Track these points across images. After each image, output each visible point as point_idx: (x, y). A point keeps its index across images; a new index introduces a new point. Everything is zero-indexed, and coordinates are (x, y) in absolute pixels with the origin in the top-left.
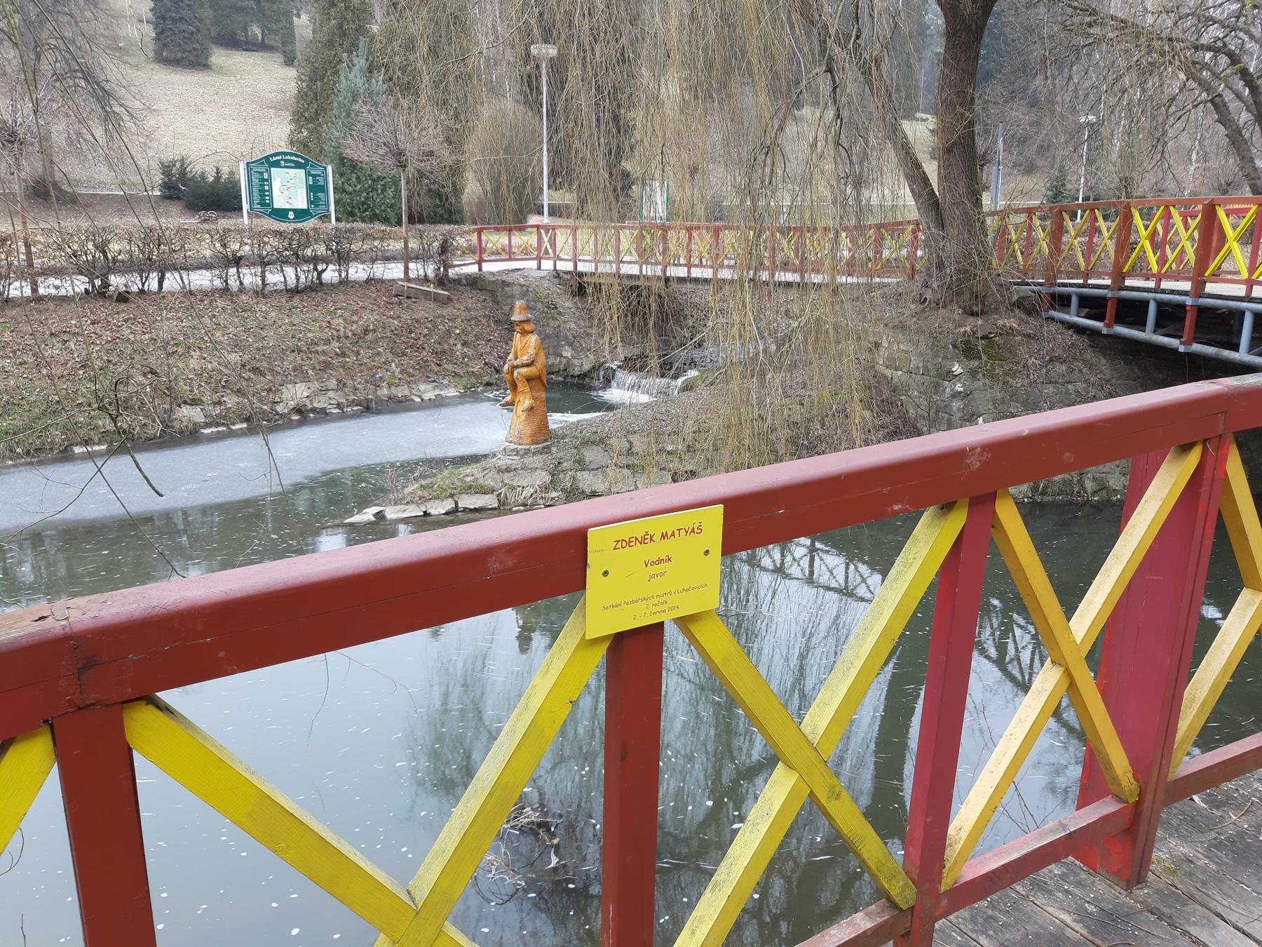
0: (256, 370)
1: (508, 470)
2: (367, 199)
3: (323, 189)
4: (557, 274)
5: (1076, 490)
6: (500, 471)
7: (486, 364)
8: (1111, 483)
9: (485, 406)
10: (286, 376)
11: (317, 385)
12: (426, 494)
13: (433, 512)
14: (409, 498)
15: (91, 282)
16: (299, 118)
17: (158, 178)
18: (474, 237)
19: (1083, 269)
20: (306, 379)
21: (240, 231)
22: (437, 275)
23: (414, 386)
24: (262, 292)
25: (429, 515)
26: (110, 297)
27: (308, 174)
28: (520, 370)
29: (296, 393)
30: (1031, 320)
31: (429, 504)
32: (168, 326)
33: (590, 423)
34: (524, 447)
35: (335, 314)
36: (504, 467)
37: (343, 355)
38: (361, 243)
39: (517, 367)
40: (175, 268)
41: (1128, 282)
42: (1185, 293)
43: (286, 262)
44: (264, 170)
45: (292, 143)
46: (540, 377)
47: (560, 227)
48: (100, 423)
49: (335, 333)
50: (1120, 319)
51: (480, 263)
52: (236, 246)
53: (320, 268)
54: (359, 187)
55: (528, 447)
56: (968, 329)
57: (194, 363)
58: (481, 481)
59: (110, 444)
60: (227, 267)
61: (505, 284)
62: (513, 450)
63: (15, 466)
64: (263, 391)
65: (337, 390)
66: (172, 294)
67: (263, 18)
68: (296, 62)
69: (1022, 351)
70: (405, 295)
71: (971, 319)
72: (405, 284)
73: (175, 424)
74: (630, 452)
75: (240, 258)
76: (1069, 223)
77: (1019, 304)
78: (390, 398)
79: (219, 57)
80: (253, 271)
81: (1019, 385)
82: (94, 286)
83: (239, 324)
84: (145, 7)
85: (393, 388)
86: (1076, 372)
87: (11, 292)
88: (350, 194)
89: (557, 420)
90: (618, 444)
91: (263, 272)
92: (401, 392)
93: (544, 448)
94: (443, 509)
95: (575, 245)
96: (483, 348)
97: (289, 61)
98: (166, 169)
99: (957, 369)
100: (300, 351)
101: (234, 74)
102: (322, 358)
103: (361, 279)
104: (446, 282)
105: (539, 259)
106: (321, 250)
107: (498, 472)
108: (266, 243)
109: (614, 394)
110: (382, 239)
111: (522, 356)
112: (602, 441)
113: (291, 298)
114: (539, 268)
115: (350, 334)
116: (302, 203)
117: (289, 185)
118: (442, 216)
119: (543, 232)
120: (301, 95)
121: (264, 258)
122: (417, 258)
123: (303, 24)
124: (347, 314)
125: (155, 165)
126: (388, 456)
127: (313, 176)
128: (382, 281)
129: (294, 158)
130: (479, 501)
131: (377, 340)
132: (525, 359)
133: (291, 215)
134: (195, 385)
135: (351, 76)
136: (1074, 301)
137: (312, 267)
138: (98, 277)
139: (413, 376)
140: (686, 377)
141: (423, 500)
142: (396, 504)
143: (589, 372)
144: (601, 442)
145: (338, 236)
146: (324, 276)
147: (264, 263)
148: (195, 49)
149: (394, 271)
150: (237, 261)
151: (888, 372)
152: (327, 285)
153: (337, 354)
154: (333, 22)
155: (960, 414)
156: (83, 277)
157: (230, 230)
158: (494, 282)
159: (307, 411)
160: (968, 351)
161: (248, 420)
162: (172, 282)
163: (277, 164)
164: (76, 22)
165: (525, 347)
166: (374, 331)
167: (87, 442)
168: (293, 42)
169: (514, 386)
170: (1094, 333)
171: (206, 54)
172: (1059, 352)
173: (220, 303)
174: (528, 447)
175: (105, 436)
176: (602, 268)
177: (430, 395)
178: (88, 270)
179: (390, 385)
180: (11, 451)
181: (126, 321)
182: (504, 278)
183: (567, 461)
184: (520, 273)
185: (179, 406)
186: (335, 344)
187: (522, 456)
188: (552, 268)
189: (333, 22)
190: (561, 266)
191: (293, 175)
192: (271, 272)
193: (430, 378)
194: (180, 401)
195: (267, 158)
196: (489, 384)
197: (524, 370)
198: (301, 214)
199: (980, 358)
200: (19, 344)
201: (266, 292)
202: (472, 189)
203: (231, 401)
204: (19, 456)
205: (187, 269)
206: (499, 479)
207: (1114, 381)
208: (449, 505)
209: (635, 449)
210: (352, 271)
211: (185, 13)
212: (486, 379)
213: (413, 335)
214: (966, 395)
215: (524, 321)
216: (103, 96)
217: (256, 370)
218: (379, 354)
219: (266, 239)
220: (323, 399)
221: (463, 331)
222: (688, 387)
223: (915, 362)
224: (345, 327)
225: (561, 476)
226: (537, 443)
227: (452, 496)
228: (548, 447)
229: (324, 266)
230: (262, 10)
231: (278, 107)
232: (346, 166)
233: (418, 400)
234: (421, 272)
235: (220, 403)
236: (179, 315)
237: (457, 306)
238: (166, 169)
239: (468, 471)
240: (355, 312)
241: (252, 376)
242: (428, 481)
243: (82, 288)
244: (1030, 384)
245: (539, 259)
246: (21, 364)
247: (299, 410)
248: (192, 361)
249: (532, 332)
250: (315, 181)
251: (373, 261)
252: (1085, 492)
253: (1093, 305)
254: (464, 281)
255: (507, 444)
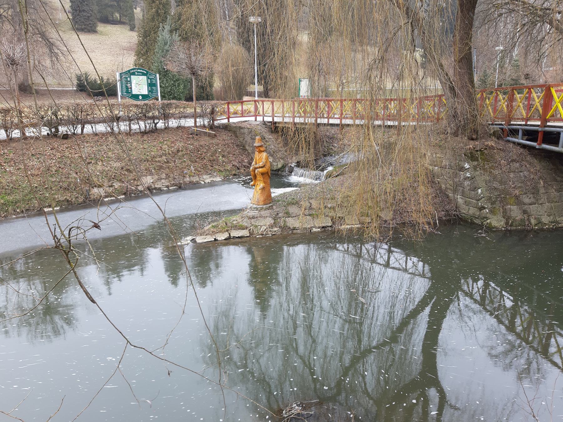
0: (128, 170)
1: (253, 218)
2: (171, 90)
3: (155, 85)
4: (264, 123)
5: (527, 223)
6: (250, 218)
7: (233, 165)
8: (543, 220)
9: (235, 185)
10: (142, 173)
11: (156, 177)
12: (215, 230)
13: (219, 239)
14: (207, 232)
15: (50, 130)
16: (139, 54)
17: (75, 82)
18: (226, 106)
19: (525, 117)
20: (151, 174)
21: (119, 105)
22: (209, 125)
23: (201, 176)
24: (129, 134)
25: (217, 240)
26: (60, 137)
27: (148, 78)
28: (258, 169)
29: (148, 180)
30: (500, 142)
31: (217, 235)
32: (87, 149)
33: (290, 194)
34: (260, 206)
35: (164, 143)
36: (252, 216)
37: (168, 162)
38: (174, 110)
39: (256, 168)
40: (89, 123)
41: (548, 124)
42: (538, 126)
43: (139, 119)
44: (127, 77)
45: (135, 65)
46: (267, 173)
47: (266, 101)
48: (56, 197)
49: (164, 152)
50: (545, 141)
51: (228, 118)
52: (117, 112)
53: (156, 121)
54: (167, 85)
55: (262, 206)
56: (471, 146)
57: (99, 167)
58: (241, 223)
59: (61, 207)
60: (113, 122)
61: (241, 128)
62: (255, 208)
63: (17, 218)
64: (131, 180)
65: (166, 179)
66: (88, 135)
67: (119, 9)
68: (136, 29)
69: (497, 157)
70: (196, 134)
71: (472, 142)
72: (195, 129)
73: (91, 196)
74: (310, 208)
75: (119, 117)
76: (518, 96)
77: (494, 134)
78: (190, 182)
79: (101, 27)
80: (125, 124)
81: (497, 173)
82: (51, 131)
83: (119, 149)
84: (68, 5)
85: (191, 177)
86: (524, 167)
87: (13, 135)
88: (164, 88)
89: (276, 192)
90: (305, 204)
91: (130, 124)
92: (195, 179)
93: (270, 207)
94: (224, 237)
95: (273, 109)
96: (231, 158)
97: (132, 29)
98: (79, 78)
99: (467, 166)
100: (148, 161)
101: (107, 35)
102: (159, 164)
103: (175, 127)
104: (214, 127)
105: (256, 116)
106: (157, 113)
107: (249, 219)
108: (131, 111)
109: (294, 179)
110: (184, 108)
111: (259, 163)
112: (297, 203)
113: (143, 136)
114: (256, 120)
115: (171, 152)
116: (146, 92)
117: (139, 83)
118: (204, 97)
119: (257, 103)
120: (140, 43)
121: (130, 117)
122: (200, 116)
123: (138, 12)
124: (169, 143)
125: (74, 76)
126: (193, 211)
127: (150, 79)
128: (184, 127)
129: (141, 71)
130: (240, 233)
131: (183, 155)
132: (261, 164)
133: (140, 97)
134: (100, 177)
135: (164, 34)
136: (520, 133)
137: (152, 121)
138: (53, 128)
139: (200, 172)
140: (327, 171)
141: (214, 233)
142: (201, 235)
143: (281, 168)
144: (296, 203)
145: (164, 107)
146: (158, 125)
147: (130, 120)
148: (90, 24)
149: (190, 123)
150: (118, 119)
151: (431, 168)
152: (159, 130)
153: (165, 162)
154: (154, 9)
155: (469, 188)
156: (46, 127)
157: (114, 105)
158: (235, 127)
159: (152, 189)
160: (472, 157)
161: (125, 194)
162: (88, 129)
163: (134, 74)
164: (37, 12)
165: (260, 159)
166: (182, 151)
167: (50, 206)
168: (134, 20)
169: (255, 177)
170: (533, 148)
171: (95, 26)
172: (515, 157)
173: (110, 139)
174: (262, 206)
175: (59, 203)
176: (286, 120)
177: (207, 181)
178: (49, 124)
179: (190, 176)
180: (14, 211)
181: (67, 148)
182: (240, 125)
183: (281, 213)
184: (247, 122)
185: (93, 188)
186: (164, 157)
187: (260, 211)
188: (262, 120)
189: (154, 9)
190: (266, 119)
191: (141, 79)
192: (133, 124)
193: (208, 172)
194: (93, 185)
195: (129, 71)
196: (235, 175)
197: (260, 170)
198: (145, 97)
199: (478, 160)
200: (17, 160)
201: (132, 134)
202: (217, 84)
203: (117, 185)
204: (18, 213)
205: (94, 123)
206: (249, 222)
207: (541, 170)
208: (226, 235)
209: (313, 206)
210: (170, 123)
211: (85, 8)
212: (234, 172)
213: (199, 153)
214: (472, 178)
215: (260, 146)
216: (50, 45)
217: (128, 170)
218: (185, 161)
219: (131, 109)
220: (159, 183)
221: (222, 150)
222: (329, 176)
223: (445, 162)
224: (168, 149)
225: (279, 220)
226: (266, 204)
227: (227, 231)
228: (272, 206)
229: (158, 121)
230: (119, 5)
231: (129, 49)
232: (165, 74)
233: (203, 183)
234: (202, 123)
235: (111, 186)
236: (91, 145)
237: (219, 138)
238: (79, 78)
239: (234, 219)
240: (172, 142)
241: (126, 173)
242: (215, 224)
243: (45, 133)
244: (502, 173)
245: (256, 116)
246: (18, 169)
247: (149, 189)
248: (98, 166)
249: (264, 151)
250: (151, 81)
251: (180, 118)
252: (531, 224)
253: (531, 135)
254: (221, 127)
255: (252, 205)
